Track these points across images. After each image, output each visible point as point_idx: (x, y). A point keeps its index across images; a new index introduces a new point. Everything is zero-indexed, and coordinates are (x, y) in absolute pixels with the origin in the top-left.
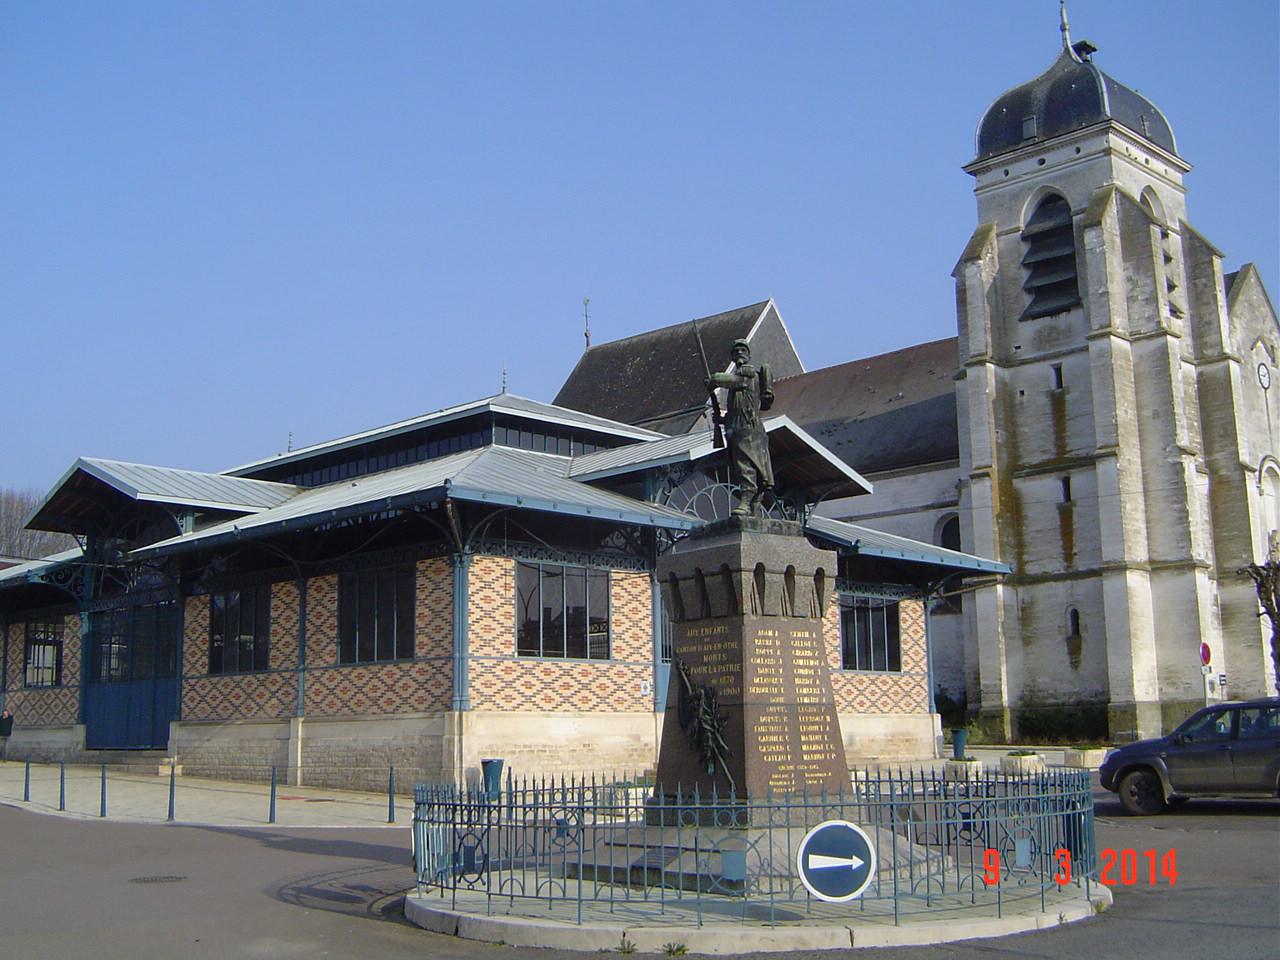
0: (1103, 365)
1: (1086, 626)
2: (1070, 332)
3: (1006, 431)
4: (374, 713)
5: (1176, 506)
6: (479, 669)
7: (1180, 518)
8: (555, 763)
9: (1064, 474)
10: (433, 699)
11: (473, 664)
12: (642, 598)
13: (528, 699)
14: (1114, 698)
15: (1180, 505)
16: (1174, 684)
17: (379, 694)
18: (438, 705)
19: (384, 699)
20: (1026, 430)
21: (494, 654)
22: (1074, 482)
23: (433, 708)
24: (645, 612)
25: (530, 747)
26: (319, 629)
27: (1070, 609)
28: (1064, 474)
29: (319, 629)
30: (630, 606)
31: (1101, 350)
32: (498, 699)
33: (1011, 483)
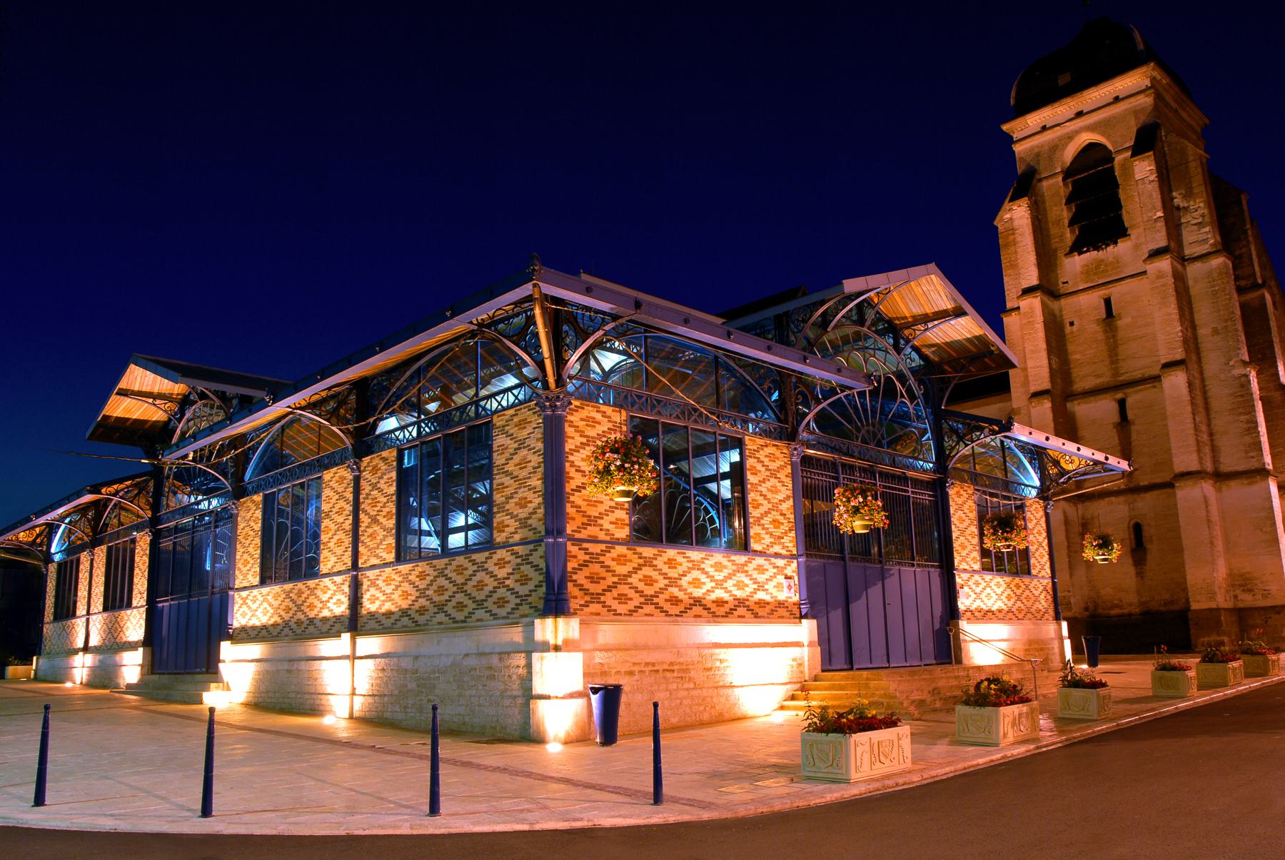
0: (1164, 285)
1: (1151, 537)
2: (1118, 262)
3: (1059, 358)
4: (440, 623)
5: (1243, 418)
6: (582, 556)
7: (1249, 429)
8: (686, 686)
9: (1119, 396)
10: (518, 601)
11: (573, 549)
12: (781, 475)
13: (649, 600)
14: (1194, 606)
15: (1247, 417)
16: (1250, 590)
17: (446, 597)
18: (525, 609)
19: (453, 603)
20: (1077, 356)
21: (602, 536)
22: (1130, 402)
23: (517, 614)
24: (536, 459)
25: (653, 665)
26: (374, 520)
27: (1133, 522)
28: (1119, 396)
29: (374, 520)
30: (768, 484)
31: (1159, 271)
32: (609, 599)
33: (1066, 407)
